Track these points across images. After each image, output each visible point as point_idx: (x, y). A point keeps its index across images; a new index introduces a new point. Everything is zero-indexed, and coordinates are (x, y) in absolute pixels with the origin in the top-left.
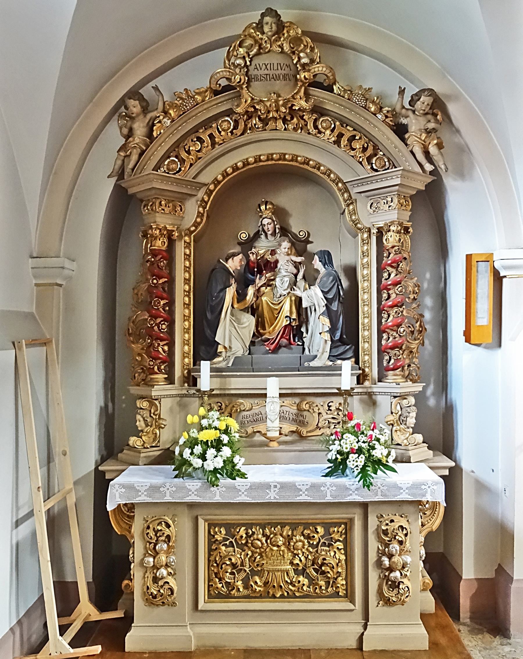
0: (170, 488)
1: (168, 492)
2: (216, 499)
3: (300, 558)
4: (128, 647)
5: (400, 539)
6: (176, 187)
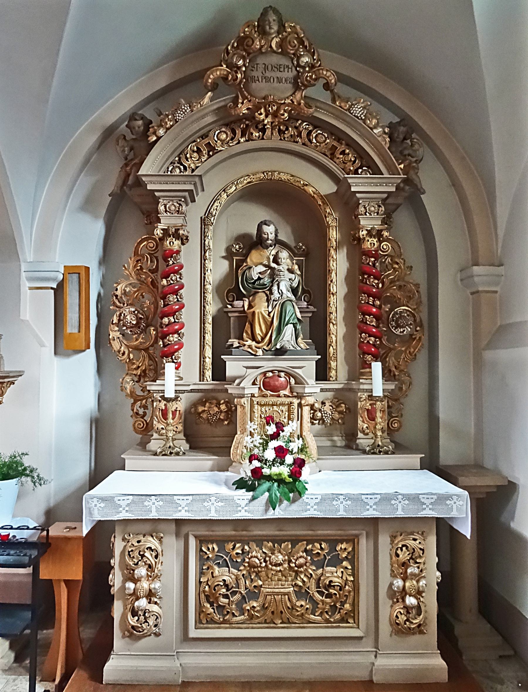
0: (402, 501)
1: (342, 506)
2: (339, 513)
3: (303, 579)
4: (106, 677)
5: (149, 562)
6: (386, 187)
